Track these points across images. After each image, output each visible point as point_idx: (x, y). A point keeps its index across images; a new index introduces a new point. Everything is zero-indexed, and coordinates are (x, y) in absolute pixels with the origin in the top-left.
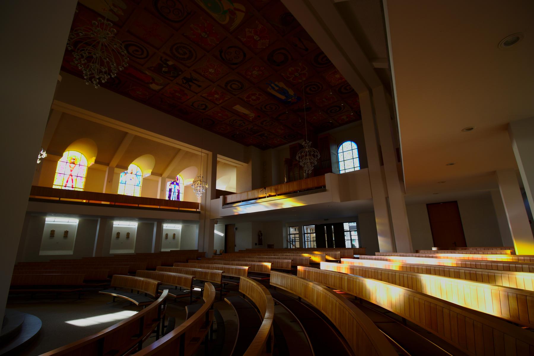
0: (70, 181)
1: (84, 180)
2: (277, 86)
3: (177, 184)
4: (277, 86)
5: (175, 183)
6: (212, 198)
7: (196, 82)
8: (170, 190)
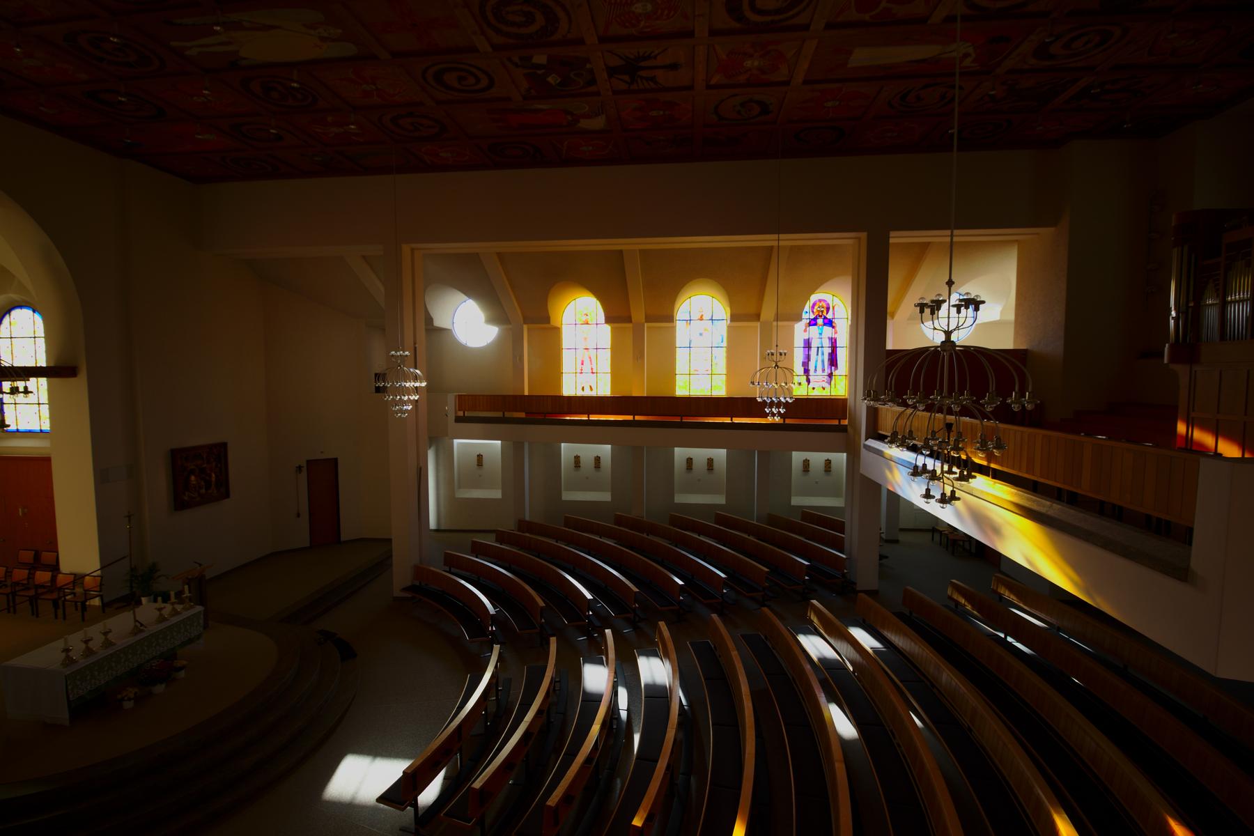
0: (587, 362)
1: (608, 353)
3: (829, 323)
5: (820, 321)
6: (180, 504)
8: (808, 344)
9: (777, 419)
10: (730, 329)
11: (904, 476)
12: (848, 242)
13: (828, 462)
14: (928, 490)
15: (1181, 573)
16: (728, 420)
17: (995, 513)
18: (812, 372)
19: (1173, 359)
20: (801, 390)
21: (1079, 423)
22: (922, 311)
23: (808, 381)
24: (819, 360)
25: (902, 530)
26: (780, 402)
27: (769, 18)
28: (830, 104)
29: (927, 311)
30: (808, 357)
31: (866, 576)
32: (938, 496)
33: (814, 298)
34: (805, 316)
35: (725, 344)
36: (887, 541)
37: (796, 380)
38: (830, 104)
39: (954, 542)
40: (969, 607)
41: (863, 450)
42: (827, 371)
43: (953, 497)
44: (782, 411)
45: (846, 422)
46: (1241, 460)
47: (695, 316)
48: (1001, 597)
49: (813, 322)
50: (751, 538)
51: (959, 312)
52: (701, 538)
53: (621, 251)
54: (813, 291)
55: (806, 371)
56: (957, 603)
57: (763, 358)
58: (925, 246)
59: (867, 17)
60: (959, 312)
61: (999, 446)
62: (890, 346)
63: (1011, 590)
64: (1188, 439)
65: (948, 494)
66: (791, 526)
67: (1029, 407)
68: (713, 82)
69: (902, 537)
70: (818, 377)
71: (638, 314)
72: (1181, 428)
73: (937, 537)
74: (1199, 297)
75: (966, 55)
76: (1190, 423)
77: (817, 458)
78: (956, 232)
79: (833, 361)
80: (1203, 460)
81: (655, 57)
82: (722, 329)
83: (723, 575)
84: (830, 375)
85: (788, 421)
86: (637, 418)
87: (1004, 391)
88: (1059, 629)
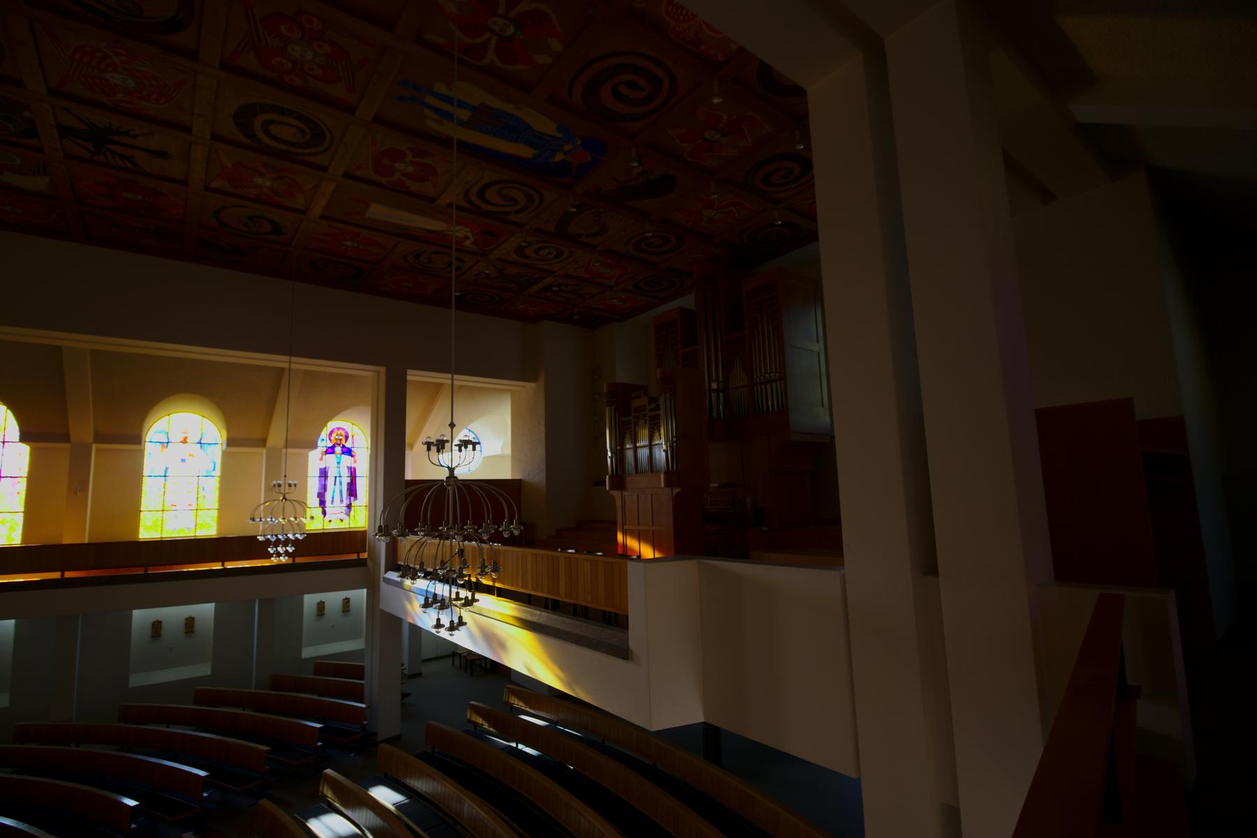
2: (462, 105)
3: (348, 451)
4: (462, 105)
5: (338, 449)
7: (116, 138)
8: (324, 474)
9: (283, 560)
10: (225, 454)
11: (419, 604)
12: (368, 375)
13: (347, 601)
14: (438, 620)
15: (623, 653)
16: (217, 566)
17: (497, 629)
18: (328, 503)
19: (612, 488)
20: (315, 523)
21: (557, 541)
22: (429, 449)
23: (324, 513)
24: (336, 491)
25: (424, 661)
26: (278, 540)
27: (284, 147)
28: (349, 243)
29: (434, 449)
30: (324, 488)
31: (388, 723)
32: (447, 625)
33: (332, 425)
34: (320, 443)
35: (218, 472)
36: (411, 676)
37: (309, 513)
38: (349, 243)
39: (472, 661)
40: (486, 726)
41: (382, 584)
42: (346, 502)
43: (461, 623)
44: (290, 549)
45: (365, 555)
46: (654, 560)
47: (176, 437)
48: (511, 707)
49: (331, 450)
50: (248, 712)
51: (460, 450)
52: (174, 729)
53: (60, 347)
54: (330, 418)
55: (322, 503)
56: (476, 724)
57: (269, 489)
58: (439, 386)
59: (383, 180)
60: (460, 450)
61: (495, 570)
62: (410, 475)
63: (520, 698)
64: (625, 546)
65: (456, 621)
66: (301, 685)
67: (516, 533)
68: (215, 185)
69: (427, 669)
70: (336, 507)
71: (82, 429)
72: (620, 537)
73: (457, 661)
74: (622, 444)
75: (466, 238)
76: (625, 533)
77: (333, 599)
78: (456, 377)
79: (352, 491)
80: (630, 564)
81: (135, 137)
82: (215, 454)
83: (202, 773)
84: (349, 506)
85: (298, 560)
86: (68, 574)
87: (498, 520)
88: (557, 724)
